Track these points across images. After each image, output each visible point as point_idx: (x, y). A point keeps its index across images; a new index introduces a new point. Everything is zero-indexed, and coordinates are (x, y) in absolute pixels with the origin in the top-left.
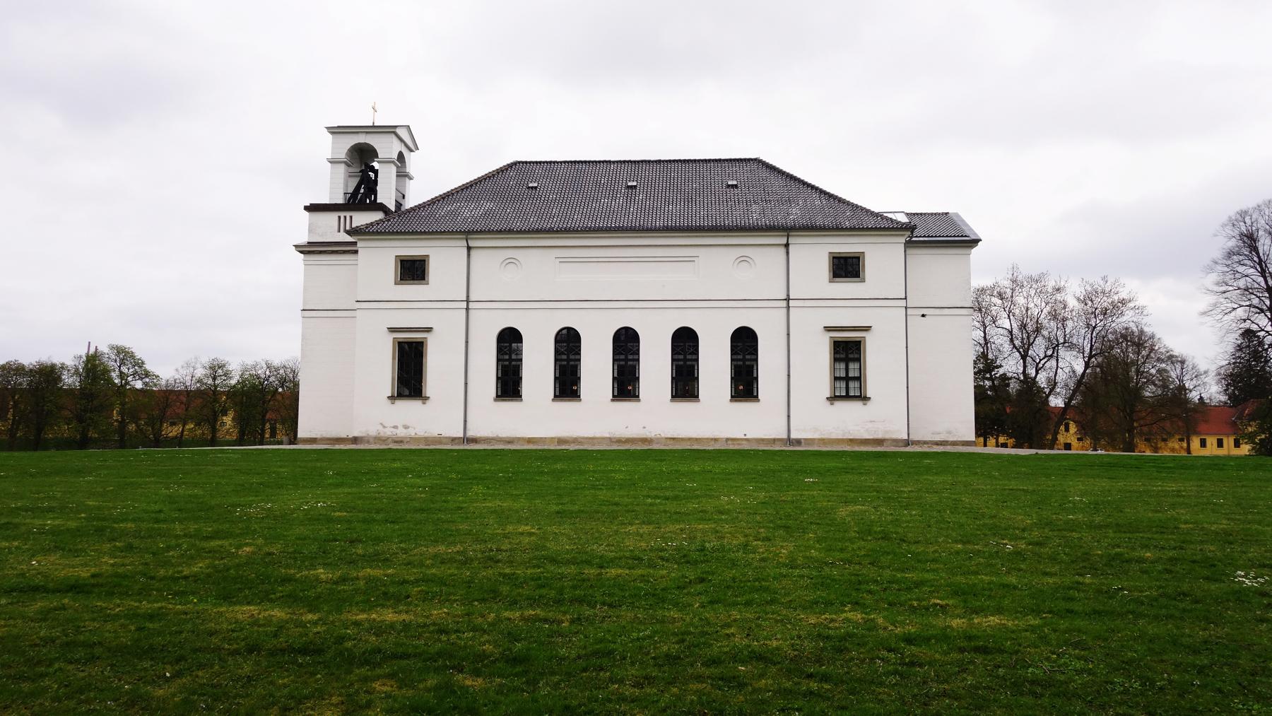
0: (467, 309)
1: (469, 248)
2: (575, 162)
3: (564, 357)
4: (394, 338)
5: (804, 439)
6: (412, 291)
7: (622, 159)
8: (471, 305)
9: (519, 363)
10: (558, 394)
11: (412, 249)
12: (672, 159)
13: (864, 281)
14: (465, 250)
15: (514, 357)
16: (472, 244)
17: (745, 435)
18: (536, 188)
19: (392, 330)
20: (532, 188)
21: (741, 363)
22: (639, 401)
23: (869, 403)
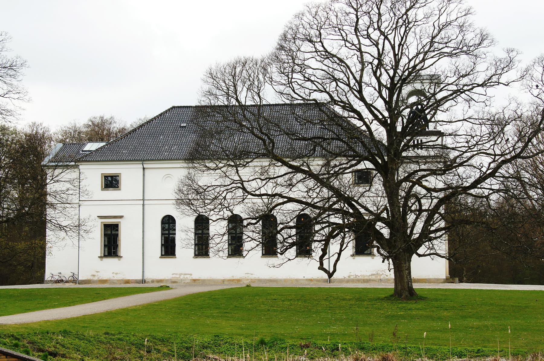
0: (143, 205)
1: (144, 169)
2: (181, 107)
3: (167, 232)
4: (101, 222)
5: (456, 283)
6: (111, 194)
7: (180, 105)
8: (146, 202)
9: (174, 236)
10: (163, 253)
11: (111, 169)
12: (186, 105)
13: (120, 190)
14: (142, 169)
15: (171, 232)
16: (145, 166)
17: (304, 277)
18: (185, 127)
19: (101, 217)
20: (183, 127)
21: (167, 236)
22: (176, 257)
23: (121, 259)
